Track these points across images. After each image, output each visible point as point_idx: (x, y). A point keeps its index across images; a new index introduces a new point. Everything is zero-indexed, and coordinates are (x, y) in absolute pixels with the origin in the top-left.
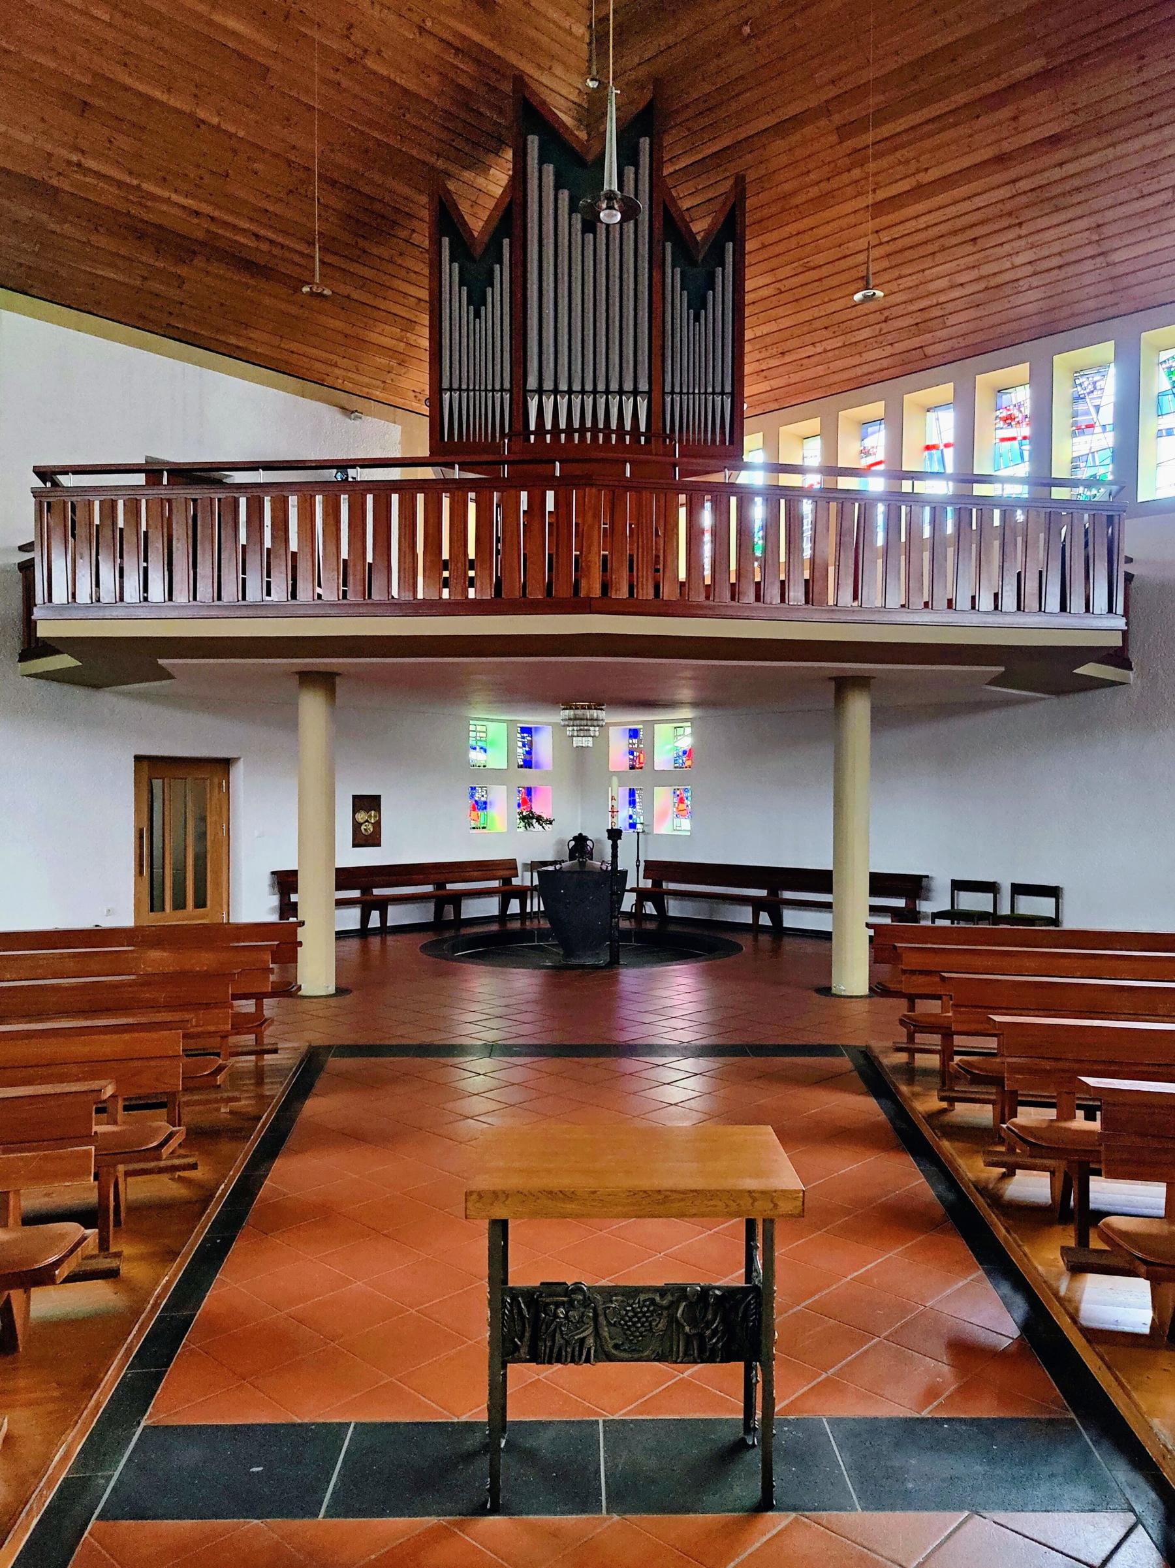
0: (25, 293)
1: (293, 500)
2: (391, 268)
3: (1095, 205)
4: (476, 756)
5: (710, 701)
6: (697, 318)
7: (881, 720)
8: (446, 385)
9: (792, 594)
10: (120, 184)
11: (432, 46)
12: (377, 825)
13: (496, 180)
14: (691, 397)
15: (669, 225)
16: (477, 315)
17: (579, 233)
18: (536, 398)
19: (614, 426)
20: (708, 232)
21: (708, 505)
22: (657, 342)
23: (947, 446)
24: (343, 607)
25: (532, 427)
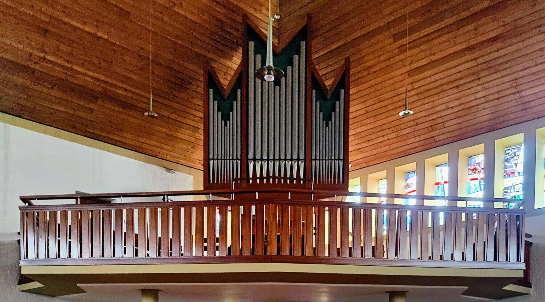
0: (21, 117)
1: (136, 211)
2: (186, 103)
3: (514, 69)
6: (327, 125)
8: (211, 157)
9: (366, 253)
10: (63, 67)
13: (236, 61)
14: (324, 161)
16: (226, 125)
17: (273, 86)
18: (253, 162)
20: (332, 85)
23: (445, 182)
24: (159, 260)
25: (251, 176)
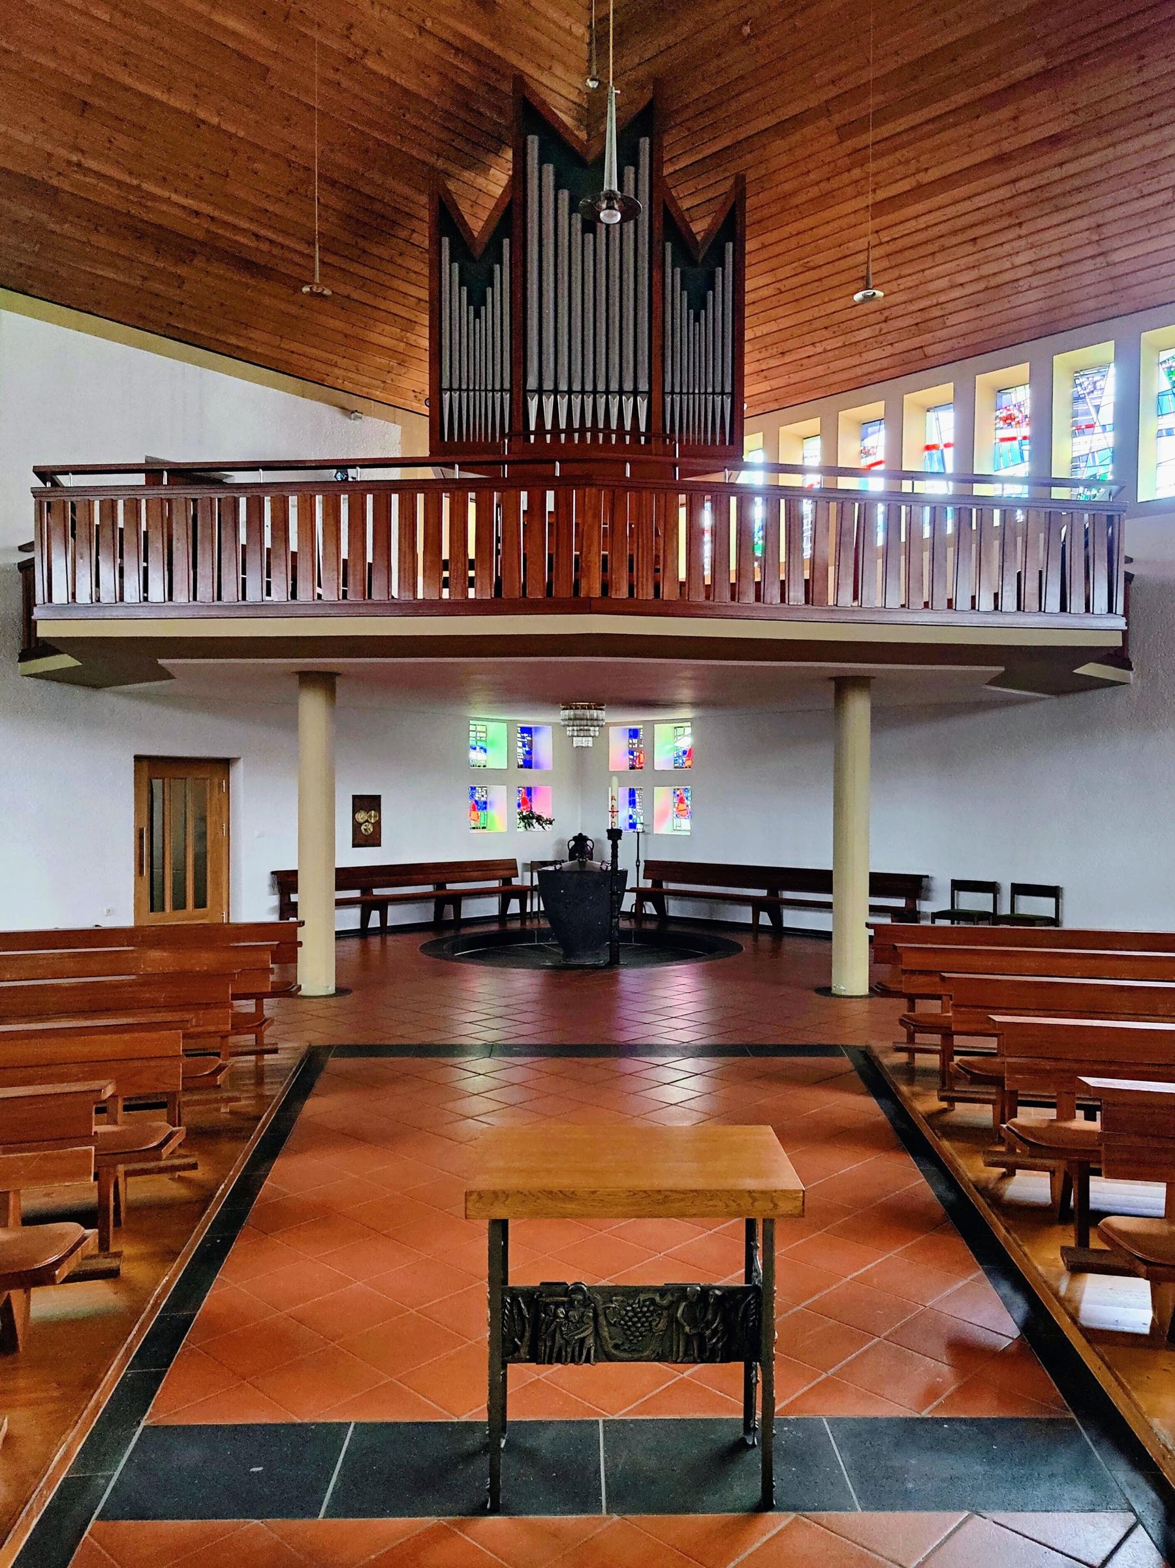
0: (25, 293)
1: (293, 500)
2: (391, 268)
3: (1095, 205)
4: (476, 756)
5: (710, 701)
6: (697, 318)
7: (881, 720)
8: (446, 385)
9: (792, 594)
10: (120, 184)
11: (432, 46)
12: (377, 825)
13: (496, 180)
14: (691, 397)
15: (669, 225)
16: (477, 315)
17: (579, 233)
18: (536, 398)
19: (614, 426)
20: (708, 232)
21: (708, 505)
22: (657, 342)
23: (947, 446)
24: (343, 607)
25: (532, 427)
